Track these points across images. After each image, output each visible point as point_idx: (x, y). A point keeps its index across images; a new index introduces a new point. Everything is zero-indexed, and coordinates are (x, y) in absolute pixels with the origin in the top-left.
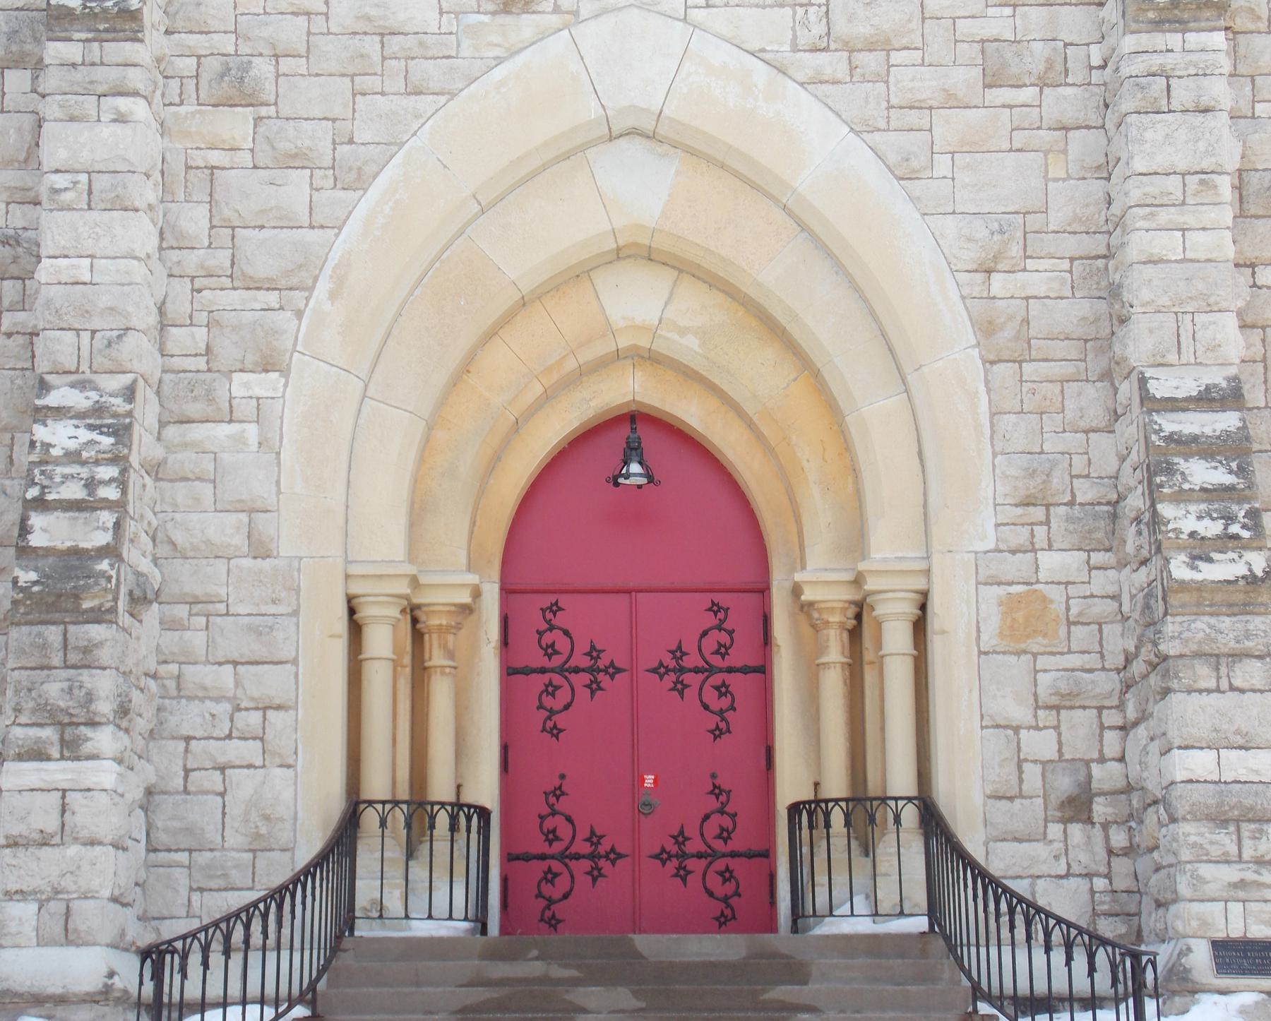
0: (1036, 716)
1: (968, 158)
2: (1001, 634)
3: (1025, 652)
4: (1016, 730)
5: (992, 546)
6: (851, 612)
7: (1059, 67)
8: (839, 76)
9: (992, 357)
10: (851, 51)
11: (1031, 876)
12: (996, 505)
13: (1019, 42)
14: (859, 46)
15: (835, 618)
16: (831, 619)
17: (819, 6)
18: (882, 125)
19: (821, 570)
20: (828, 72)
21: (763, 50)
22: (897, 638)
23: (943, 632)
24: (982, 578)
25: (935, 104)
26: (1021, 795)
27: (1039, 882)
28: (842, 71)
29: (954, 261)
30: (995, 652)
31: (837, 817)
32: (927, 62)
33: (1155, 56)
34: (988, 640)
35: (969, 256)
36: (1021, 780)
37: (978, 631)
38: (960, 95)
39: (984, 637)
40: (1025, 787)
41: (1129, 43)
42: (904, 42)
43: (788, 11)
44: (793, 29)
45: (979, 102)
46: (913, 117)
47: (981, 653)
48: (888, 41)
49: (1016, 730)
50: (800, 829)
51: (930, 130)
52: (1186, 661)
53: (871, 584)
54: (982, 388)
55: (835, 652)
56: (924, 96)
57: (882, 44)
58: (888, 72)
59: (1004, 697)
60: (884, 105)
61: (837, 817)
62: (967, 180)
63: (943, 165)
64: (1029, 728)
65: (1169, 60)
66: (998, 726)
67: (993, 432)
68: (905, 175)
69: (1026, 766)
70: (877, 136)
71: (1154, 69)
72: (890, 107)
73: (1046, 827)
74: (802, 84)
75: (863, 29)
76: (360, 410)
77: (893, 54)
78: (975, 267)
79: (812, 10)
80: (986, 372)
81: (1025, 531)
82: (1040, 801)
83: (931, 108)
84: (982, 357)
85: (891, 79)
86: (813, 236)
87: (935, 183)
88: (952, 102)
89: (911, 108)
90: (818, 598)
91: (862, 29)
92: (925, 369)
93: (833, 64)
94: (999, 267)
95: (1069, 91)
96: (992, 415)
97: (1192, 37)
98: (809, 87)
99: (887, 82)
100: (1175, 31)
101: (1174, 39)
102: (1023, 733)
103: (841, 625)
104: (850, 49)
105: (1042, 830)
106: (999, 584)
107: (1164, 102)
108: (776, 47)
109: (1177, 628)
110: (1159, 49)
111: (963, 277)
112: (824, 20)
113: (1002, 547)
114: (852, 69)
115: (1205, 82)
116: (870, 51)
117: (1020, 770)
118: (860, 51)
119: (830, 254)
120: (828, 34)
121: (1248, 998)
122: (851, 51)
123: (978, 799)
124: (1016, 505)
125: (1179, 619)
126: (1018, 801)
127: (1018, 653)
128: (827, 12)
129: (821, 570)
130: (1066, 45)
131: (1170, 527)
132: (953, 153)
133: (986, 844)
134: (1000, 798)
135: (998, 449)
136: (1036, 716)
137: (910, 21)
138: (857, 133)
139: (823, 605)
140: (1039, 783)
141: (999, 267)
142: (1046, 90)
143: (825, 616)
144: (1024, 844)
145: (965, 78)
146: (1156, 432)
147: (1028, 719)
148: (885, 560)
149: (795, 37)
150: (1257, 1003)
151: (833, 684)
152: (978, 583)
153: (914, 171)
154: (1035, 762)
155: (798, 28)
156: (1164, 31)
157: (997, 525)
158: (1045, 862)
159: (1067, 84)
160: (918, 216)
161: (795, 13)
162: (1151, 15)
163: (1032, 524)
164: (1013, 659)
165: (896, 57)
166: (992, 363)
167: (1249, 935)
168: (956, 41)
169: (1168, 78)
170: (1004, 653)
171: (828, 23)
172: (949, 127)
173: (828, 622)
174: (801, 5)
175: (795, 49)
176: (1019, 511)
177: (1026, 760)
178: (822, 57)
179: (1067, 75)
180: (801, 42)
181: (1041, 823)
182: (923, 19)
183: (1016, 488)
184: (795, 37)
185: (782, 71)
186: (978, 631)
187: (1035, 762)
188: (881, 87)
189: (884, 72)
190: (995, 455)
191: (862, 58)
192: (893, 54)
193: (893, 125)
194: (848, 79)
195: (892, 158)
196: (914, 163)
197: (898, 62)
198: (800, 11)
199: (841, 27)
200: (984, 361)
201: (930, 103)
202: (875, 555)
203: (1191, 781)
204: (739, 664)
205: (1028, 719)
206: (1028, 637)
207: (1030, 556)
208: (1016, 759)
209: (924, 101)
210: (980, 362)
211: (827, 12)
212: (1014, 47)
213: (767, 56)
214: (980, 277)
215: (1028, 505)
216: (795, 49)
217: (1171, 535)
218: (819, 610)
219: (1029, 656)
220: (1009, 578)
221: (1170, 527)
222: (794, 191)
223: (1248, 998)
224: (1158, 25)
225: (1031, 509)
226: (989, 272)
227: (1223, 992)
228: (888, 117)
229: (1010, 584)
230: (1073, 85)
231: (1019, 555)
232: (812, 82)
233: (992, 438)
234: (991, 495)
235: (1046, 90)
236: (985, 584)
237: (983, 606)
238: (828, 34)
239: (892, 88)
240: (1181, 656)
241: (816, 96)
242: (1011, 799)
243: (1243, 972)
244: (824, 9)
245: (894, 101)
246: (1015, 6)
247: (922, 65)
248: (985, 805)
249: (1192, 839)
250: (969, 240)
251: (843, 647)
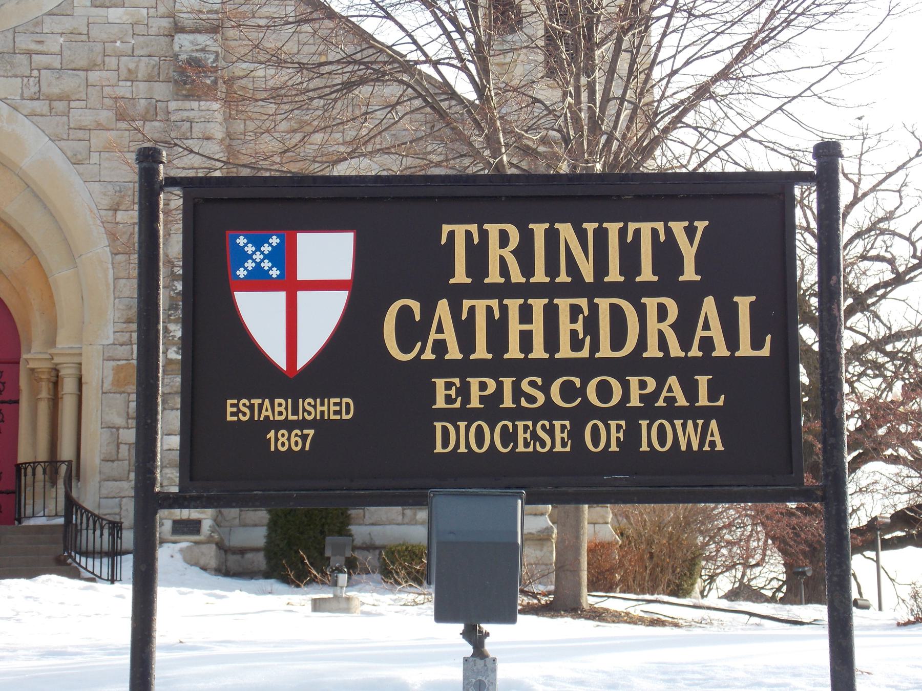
0: (127, 422)
1: (107, 155)
2: (113, 384)
3: (124, 392)
4: (118, 429)
5: (111, 342)
6: (53, 373)
7: (152, 112)
8: (44, 113)
9: (115, 252)
10: (50, 101)
11: (120, 497)
12: (114, 322)
13: (134, 99)
14: (55, 98)
15: (44, 376)
16: (43, 377)
17: (35, 77)
18: (65, 137)
19: (37, 353)
20: (38, 110)
21: (6, 99)
22: (68, 386)
23: (87, 383)
24: (105, 358)
25: (92, 128)
26: (118, 460)
27: (124, 500)
28: (46, 109)
29: (98, 204)
30: (111, 393)
31: (39, 470)
32: (88, 107)
33: (185, 112)
34: (107, 386)
35: (105, 202)
36: (118, 452)
37: (103, 382)
38: (104, 124)
39: (105, 385)
40: (120, 455)
41: (173, 105)
42: (77, 97)
43: (19, 80)
44: (22, 88)
45: (114, 127)
46: (80, 134)
47: (103, 393)
48: (68, 96)
49: (118, 429)
50: (25, 475)
51: (89, 140)
52: (171, 396)
53: (57, 360)
54: (110, 266)
55: (44, 394)
56: (86, 124)
57: (65, 98)
58: (69, 111)
59: (112, 413)
60: (67, 127)
61: (39, 470)
62: (107, 165)
63: (95, 157)
64: (124, 428)
65: (191, 114)
66: (109, 427)
67: (115, 287)
68: (76, 162)
69: (122, 446)
70: (62, 143)
71: (184, 118)
72: (70, 129)
73: (129, 474)
74: (25, 116)
75: (56, 90)
76: (60, 228)
77: (72, 103)
78: (108, 208)
79: (32, 79)
80: (113, 258)
81: (128, 335)
82: (127, 462)
83: (90, 130)
84: (111, 251)
85: (70, 115)
86: (33, 191)
87: (91, 166)
88: (100, 127)
89: (80, 129)
90: (36, 367)
91: (55, 90)
92: (83, 257)
93: (40, 106)
94: (121, 208)
95: (157, 124)
96: (115, 279)
97: (202, 103)
98: (29, 117)
99: (68, 116)
100: (195, 100)
101: (195, 104)
102: (121, 431)
103: (49, 380)
104: (50, 99)
105: (127, 475)
106: (114, 360)
107: (189, 134)
108: (13, 97)
109: (169, 381)
110: (187, 108)
111: (103, 213)
112: (38, 85)
113: (116, 342)
114: (51, 109)
115: (208, 125)
116: (60, 100)
117: (118, 448)
118: (55, 100)
119: (40, 200)
120: (39, 91)
121: (184, 545)
122: (50, 101)
123: (97, 461)
124: (124, 323)
125: (169, 377)
126: (116, 462)
127: (121, 393)
128: (39, 81)
129: (37, 353)
130: (157, 101)
131: (171, 334)
132: (100, 152)
133: (100, 482)
134: (108, 461)
135: (116, 296)
136: (127, 422)
137: (79, 87)
138: (53, 141)
139: (39, 370)
140: (127, 454)
141: (121, 208)
142: (147, 123)
143: (40, 376)
144: (118, 482)
145: (106, 116)
146: (174, 290)
147: (124, 423)
148: (63, 348)
149: (22, 92)
150: (188, 547)
151: (43, 408)
152: (104, 360)
153: (80, 161)
154: (125, 444)
155: (24, 88)
156: (190, 100)
157: (115, 332)
158: (127, 490)
159: (157, 120)
160: (82, 182)
161: (23, 80)
162: (184, 92)
163: (131, 332)
164: (118, 396)
165: (73, 104)
166: (116, 254)
167: (191, 518)
168: (103, 97)
169: (191, 122)
170: (114, 393)
171: (40, 86)
172: (98, 139)
173: (41, 379)
174: (26, 77)
175: (22, 98)
176: (125, 325)
177: (121, 443)
178: (36, 103)
179: (156, 116)
180: (25, 95)
181: (126, 472)
182: (87, 86)
183: (122, 315)
184: (22, 92)
185: (15, 109)
186: (103, 382)
187: (125, 444)
188: (65, 118)
189: (66, 111)
190: (115, 298)
191: (56, 104)
192: (72, 103)
193: (71, 137)
194: (49, 114)
195: (69, 154)
196: (79, 157)
197: (74, 106)
198: (26, 80)
199: (44, 89)
200: (112, 254)
201: (89, 127)
202: (59, 346)
203: (170, 450)
204: (7, 399)
205: (124, 423)
206: (126, 385)
207: (129, 347)
208: (116, 443)
209: (86, 126)
210: (109, 254)
211: (39, 81)
212: (132, 101)
213: (8, 102)
214: (111, 213)
215: (130, 322)
216: (22, 98)
217: (170, 338)
218: (37, 372)
219: (126, 394)
220: (118, 357)
221: (171, 334)
222: (21, 168)
223: (184, 545)
224: (187, 97)
225: (131, 325)
226: (116, 210)
227: (175, 542)
228: (69, 134)
229: (119, 360)
230: (160, 121)
231: (124, 347)
232: (30, 115)
233: (114, 291)
234: (112, 318)
235: (147, 123)
236: (107, 360)
237: (105, 371)
238: (39, 91)
239: (71, 119)
240: (170, 393)
241: (32, 122)
242: (113, 461)
243: (184, 533)
244: (37, 79)
245: (72, 126)
246: (132, 81)
247: (86, 108)
248: (100, 464)
249: (169, 475)
250: (105, 195)
251: (49, 389)
